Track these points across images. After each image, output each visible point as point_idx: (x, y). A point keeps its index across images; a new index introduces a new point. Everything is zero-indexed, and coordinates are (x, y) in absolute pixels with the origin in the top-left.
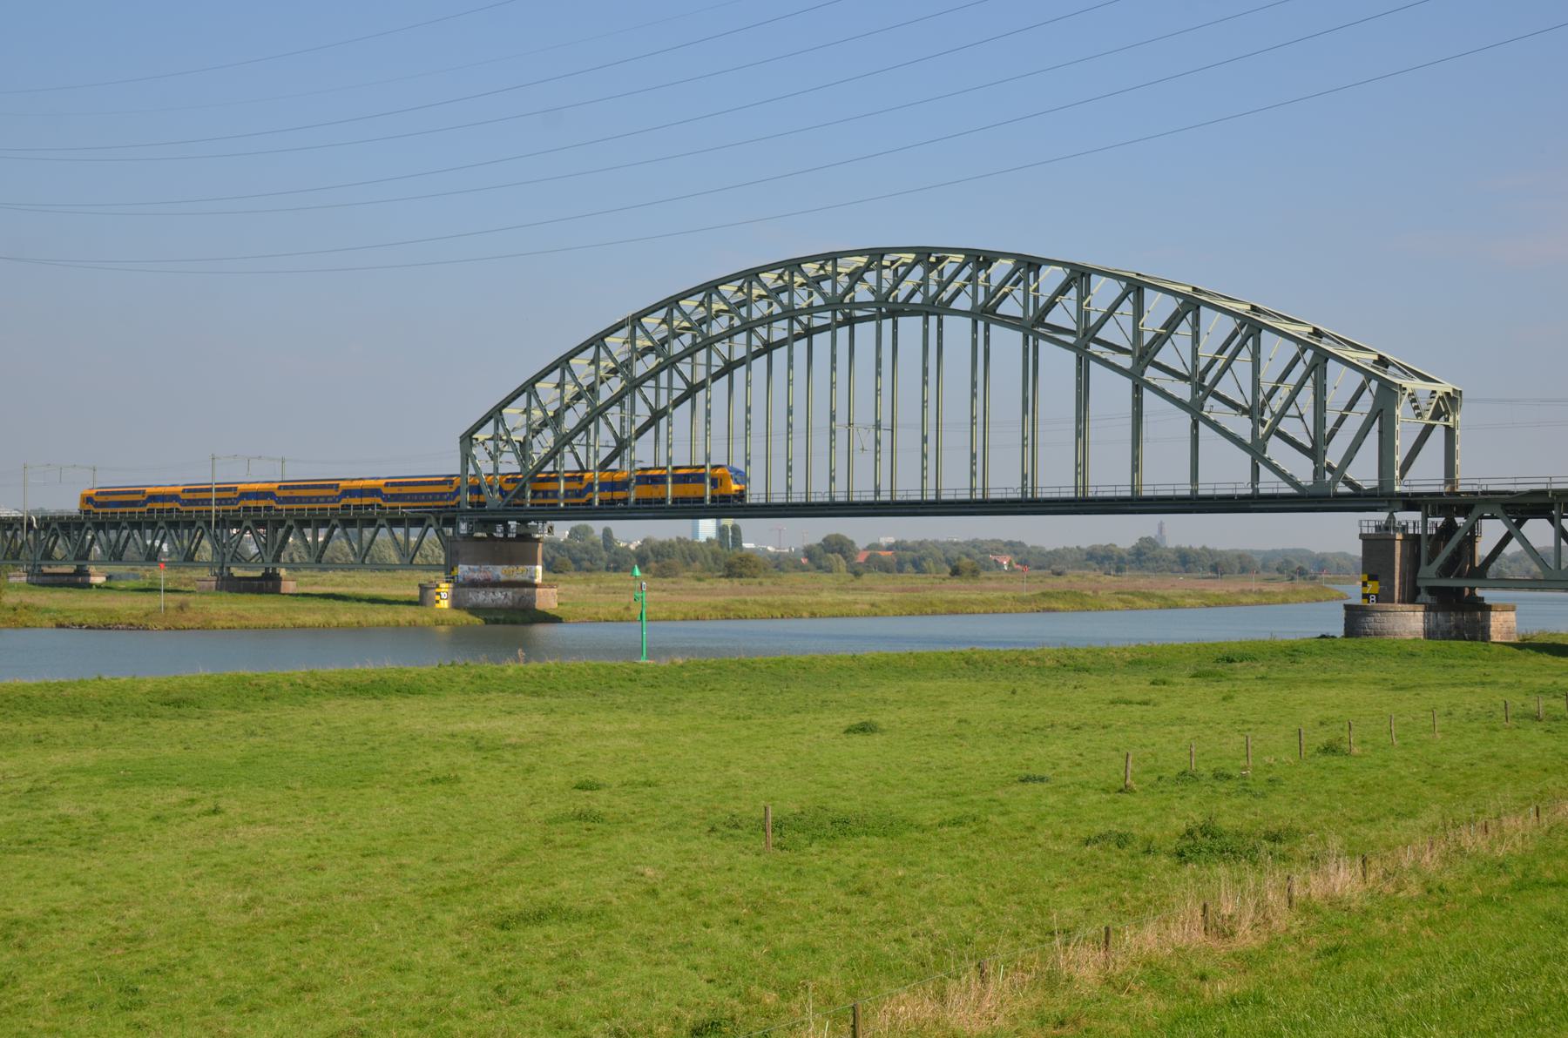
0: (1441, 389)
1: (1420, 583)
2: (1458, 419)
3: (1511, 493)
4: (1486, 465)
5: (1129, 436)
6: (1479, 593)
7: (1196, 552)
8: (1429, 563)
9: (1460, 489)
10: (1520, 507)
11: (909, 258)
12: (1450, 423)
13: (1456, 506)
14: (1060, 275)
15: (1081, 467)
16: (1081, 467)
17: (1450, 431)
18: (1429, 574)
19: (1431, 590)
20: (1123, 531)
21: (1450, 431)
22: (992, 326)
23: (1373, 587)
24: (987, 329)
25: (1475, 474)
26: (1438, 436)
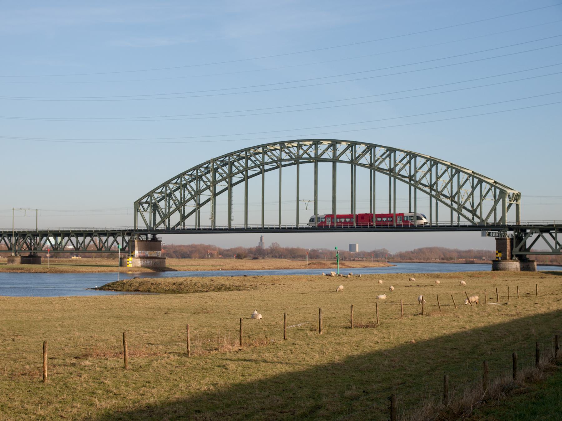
0: (516, 192)
1: (513, 254)
2: (520, 202)
3: (541, 225)
4: (528, 217)
5: (248, 205)
6: (527, 256)
7: (296, 249)
8: (516, 247)
9: (521, 224)
10: (544, 229)
11: (311, 143)
12: (518, 203)
13: (521, 230)
14: (363, 147)
15: (230, 219)
16: (230, 219)
17: (517, 206)
18: (516, 250)
19: (517, 256)
20: (249, 241)
21: (517, 206)
22: (376, 172)
23: (500, 255)
24: (374, 172)
25: (525, 220)
26: (513, 207)
